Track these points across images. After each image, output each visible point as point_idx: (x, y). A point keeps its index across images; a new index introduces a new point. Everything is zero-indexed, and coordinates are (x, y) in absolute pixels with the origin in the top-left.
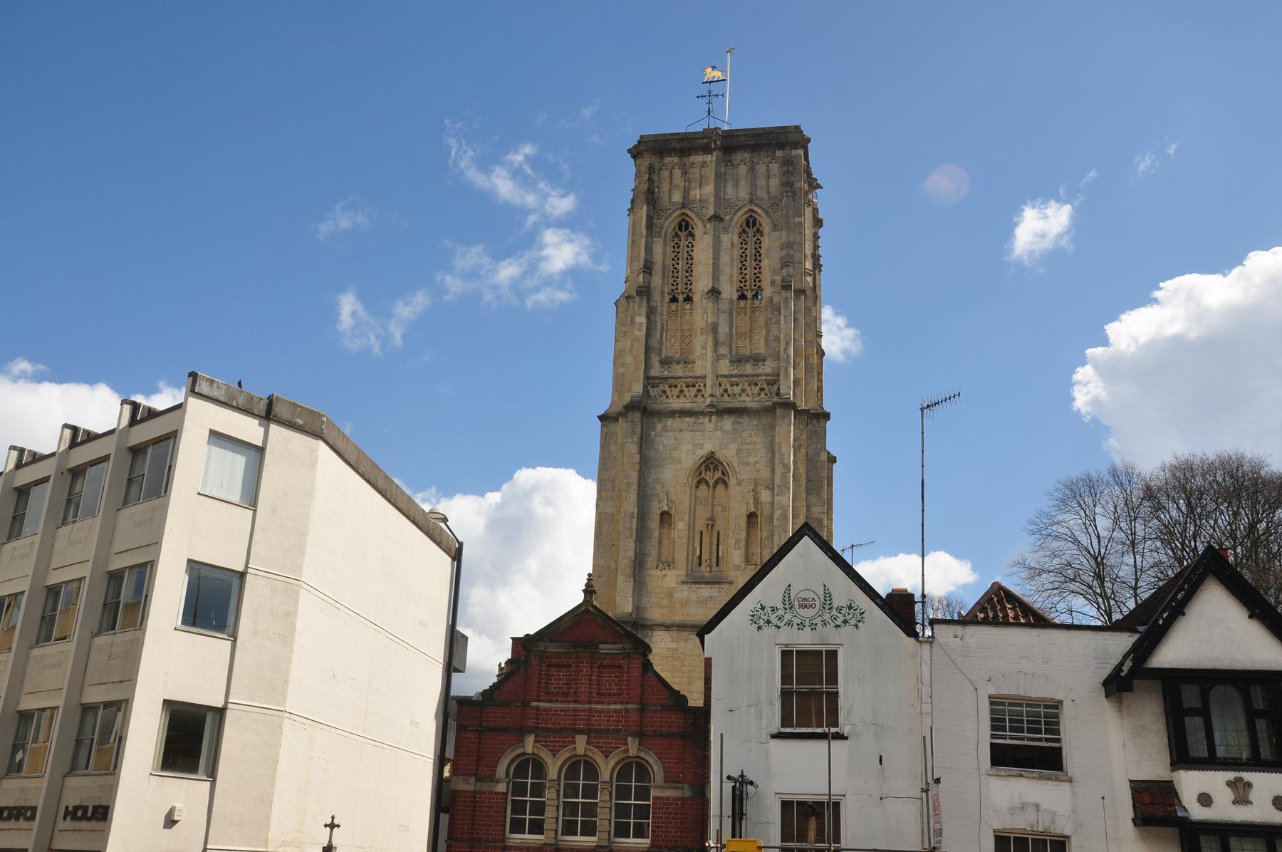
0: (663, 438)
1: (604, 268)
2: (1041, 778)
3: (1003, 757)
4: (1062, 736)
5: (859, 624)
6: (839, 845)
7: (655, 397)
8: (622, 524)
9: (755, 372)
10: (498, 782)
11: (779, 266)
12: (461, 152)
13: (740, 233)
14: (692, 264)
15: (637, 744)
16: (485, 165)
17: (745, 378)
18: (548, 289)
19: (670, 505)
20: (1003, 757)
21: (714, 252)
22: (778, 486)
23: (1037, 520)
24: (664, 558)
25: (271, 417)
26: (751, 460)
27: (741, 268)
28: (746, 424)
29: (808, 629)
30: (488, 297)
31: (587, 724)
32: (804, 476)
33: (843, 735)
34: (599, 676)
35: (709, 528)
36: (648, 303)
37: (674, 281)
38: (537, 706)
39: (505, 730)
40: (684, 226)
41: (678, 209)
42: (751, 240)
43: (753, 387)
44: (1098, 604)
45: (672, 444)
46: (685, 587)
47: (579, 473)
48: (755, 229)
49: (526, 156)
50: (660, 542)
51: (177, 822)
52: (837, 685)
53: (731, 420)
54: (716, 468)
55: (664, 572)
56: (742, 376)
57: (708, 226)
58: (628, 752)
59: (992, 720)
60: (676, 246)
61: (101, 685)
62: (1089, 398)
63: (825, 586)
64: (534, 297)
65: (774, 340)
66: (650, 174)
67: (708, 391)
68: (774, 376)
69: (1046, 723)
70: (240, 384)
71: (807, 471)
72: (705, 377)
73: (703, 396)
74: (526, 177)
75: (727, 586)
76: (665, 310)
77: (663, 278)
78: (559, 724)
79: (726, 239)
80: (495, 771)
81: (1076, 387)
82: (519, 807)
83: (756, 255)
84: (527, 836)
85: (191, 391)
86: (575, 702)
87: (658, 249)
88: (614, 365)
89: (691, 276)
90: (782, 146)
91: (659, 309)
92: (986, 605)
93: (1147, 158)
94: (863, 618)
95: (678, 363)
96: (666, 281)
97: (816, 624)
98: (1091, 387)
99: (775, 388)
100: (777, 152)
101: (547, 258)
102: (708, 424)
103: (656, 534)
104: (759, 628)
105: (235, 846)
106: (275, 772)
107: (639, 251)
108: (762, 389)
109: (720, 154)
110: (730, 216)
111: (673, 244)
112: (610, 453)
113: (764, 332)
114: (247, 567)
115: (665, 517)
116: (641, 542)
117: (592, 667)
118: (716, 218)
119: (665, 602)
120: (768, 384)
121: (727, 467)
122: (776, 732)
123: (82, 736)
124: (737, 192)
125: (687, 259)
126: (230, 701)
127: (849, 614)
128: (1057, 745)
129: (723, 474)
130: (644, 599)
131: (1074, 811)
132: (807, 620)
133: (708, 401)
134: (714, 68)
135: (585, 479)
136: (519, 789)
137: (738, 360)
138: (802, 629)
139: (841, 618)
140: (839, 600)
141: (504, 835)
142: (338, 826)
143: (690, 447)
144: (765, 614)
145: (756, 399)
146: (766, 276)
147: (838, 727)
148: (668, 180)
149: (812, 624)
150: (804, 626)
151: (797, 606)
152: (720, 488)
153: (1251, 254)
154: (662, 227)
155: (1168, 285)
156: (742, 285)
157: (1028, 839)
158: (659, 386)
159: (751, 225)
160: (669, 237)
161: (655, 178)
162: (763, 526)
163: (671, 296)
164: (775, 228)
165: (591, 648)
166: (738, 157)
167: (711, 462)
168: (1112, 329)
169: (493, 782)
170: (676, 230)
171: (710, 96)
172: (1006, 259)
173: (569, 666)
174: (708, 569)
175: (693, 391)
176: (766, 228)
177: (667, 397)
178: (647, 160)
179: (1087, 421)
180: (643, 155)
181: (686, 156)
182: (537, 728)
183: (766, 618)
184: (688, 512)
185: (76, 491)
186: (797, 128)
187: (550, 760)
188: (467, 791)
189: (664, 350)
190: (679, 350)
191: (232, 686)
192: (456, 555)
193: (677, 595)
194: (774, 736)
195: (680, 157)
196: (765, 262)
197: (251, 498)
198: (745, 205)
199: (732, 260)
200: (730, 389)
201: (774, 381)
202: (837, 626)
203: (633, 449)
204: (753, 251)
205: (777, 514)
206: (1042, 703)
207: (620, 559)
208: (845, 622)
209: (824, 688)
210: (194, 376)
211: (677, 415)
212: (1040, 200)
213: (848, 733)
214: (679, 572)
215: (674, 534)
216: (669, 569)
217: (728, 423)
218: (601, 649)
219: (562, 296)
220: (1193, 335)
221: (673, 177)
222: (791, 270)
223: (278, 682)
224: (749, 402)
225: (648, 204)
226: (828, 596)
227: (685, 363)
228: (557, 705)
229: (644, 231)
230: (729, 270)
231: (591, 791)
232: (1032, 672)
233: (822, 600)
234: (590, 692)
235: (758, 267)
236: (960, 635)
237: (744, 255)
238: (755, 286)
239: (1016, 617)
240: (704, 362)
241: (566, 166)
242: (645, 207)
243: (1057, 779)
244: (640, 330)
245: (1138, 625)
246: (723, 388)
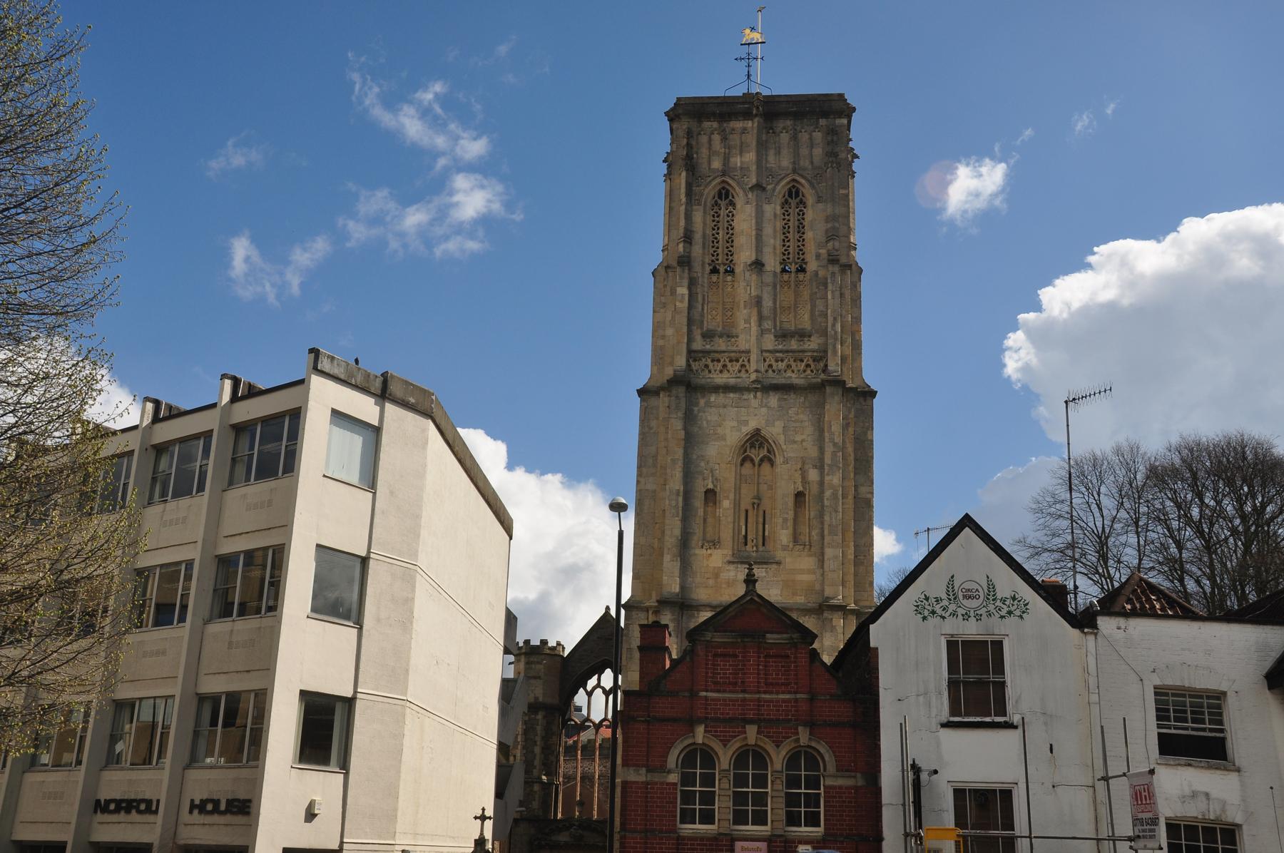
0: (706, 414)
1: (518, 217)
2: (1210, 767)
3: (1171, 747)
4: (1226, 726)
5: (1024, 615)
6: (1013, 832)
7: (697, 371)
8: (667, 502)
9: (801, 348)
10: (669, 772)
11: (824, 240)
12: (366, 88)
14: (733, 234)
15: (808, 733)
16: (392, 102)
17: (791, 354)
18: (459, 238)
19: (715, 483)
20: (1171, 747)
21: (757, 223)
22: (829, 465)
23: (1041, 499)
24: (709, 536)
25: (387, 395)
26: (798, 438)
27: (784, 240)
28: (792, 401)
29: (973, 620)
30: (394, 244)
31: (758, 714)
32: (852, 455)
33: (1012, 724)
34: (765, 666)
35: (755, 507)
36: (689, 274)
37: (714, 252)
38: (706, 697)
39: (674, 720)
40: (724, 194)
41: (718, 176)
42: (793, 211)
43: (799, 363)
44: (1102, 585)
45: (716, 421)
46: (732, 567)
47: (488, 434)
48: (798, 199)
49: (436, 94)
50: (705, 520)
51: (316, 815)
52: (1004, 675)
53: (777, 397)
54: (761, 446)
55: (709, 551)
56: (787, 351)
57: (750, 195)
58: (799, 742)
59: (1158, 710)
60: (716, 215)
61: (222, 675)
62: (1020, 364)
63: (988, 577)
64: (443, 247)
65: (820, 315)
66: (688, 139)
67: (753, 367)
68: (820, 352)
69: (1192, 712)
70: (357, 361)
71: (855, 450)
72: (748, 352)
73: (747, 371)
74: (436, 118)
75: (774, 566)
76: (706, 281)
77: (704, 247)
78: (728, 714)
79: (768, 209)
80: (666, 761)
81: (1007, 354)
82: (688, 797)
83: (799, 227)
84: (698, 826)
85: (313, 368)
86: (744, 691)
87: (698, 217)
88: (653, 337)
89: (732, 246)
90: (825, 114)
91: (700, 280)
92: (1131, 596)
93: (1085, 117)
94: (1027, 609)
95: (721, 336)
96: (706, 251)
97: (981, 615)
98: (1022, 353)
99: (822, 365)
100: (820, 120)
101: (457, 204)
102: (753, 400)
103: (701, 512)
104: (924, 618)
105: (367, 839)
106: (401, 763)
107: (679, 219)
108: (808, 366)
109: (761, 120)
110: (773, 185)
111: (712, 213)
112: (650, 428)
113: (809, 307)
114: (369, 552)
115: (711, 495)
116: (685, 521)
117: (759, 657)
118: (759, 187)
119: (711, 582)
120: (814, 361)
121: (773, 444)
122: (946, 721)
123: (199, 727)
124: (779, 160)
125: (728, 228)
126: (359, 690)
127: (1013, 605)
128: (1221, 735)
129: (769, 451)
130: (690, 579)
131: (1244, 801)
132: (972, 611)
133: (753, 377)
134: (752, 29)
135: (495, 440)
136: (687, 779)
137: (783, 335)
138: (967, 620)
139: (1005, 609)
140: (1003, 591)
141: (676, 825)
142: (476, 818)
143: (735, 424)
144: (929, 605)
145: (802, 376)
146: (811, 249)
147: (1006, 716)
148: (706, 145)
149: (977, 614)
150: (969, 617)
151: (961, 597)
152: (766, 466)
153: (1185, 220)
154: (702, 195)
155: (1102, 249)
156: (785, 257)
157: (1180, 825)
158: (700, 360)
159: (794, 196)
160: (709, 204)
161: (694, 143)
162: (811, 505)
163: (711, 267)
164: (819, 200)
165: (759, 638)
166: (779, 124)
167: (756, 439)
168: (1046, 294)
169: (664, 772)
170: (716, 198)
171: (749, 59)
172: (938, 218)
173: (735, 656)
174: (755, 549)
175: (737, 366)
176: (810, 200)
177: (710, 372)
178: (684, 125)
179: (1017, 388)
180: (680, 118)
181: (725, 121)
182: (707, 718)
183: (930, 608)
184: (733, 490)
185: (160, 471)
186: (841, 96)
187: (721, 750)
189: (705, 322)
190: (721, 323)
191: (360, 676)
194: (944, 725)
195: (719, 122)
196: (809, 235)
197: (370, 481)
198: (788, 175)
199: (775, 231)
200: (774, 364)
201: (821, 357)
202: (1002, 617)
203: (677, 425)
204: (797, 223)
205: (828, 493)
206: (1187, 693)
207: (667, 538)
208: (1010, 613)
209: (992, 677)
210: (315, 352)
211: (721, 391)
212: (974, 157)
213: (1017, 722)
214: (725, 552)
215: (720, 512)
216: (715, 548)
217: (773, 400)
218: (768, 639)
219: (473, 246)
220: (1126, 302)
221: (712, 142)
222: (837, 244)
223: (399, 673)
224: (795, 378)
225: (687, 170)
226: (991, 587)
227: (728, 336)
228: (726, 695)
229: (684, 200)
230: (772, 241)
231: (761, 781)
232: (1195, 664)
233: (986, 591)
234: (758, 682)
235: (801, 240)
236: (1123, 627)
237: (787, 226)
238: (798, 259)
239: (1163, 609)
240: (749, 335)
241: (479, 107)
242: (684, 174)
243: (1226, 769)
244: (682, 301)
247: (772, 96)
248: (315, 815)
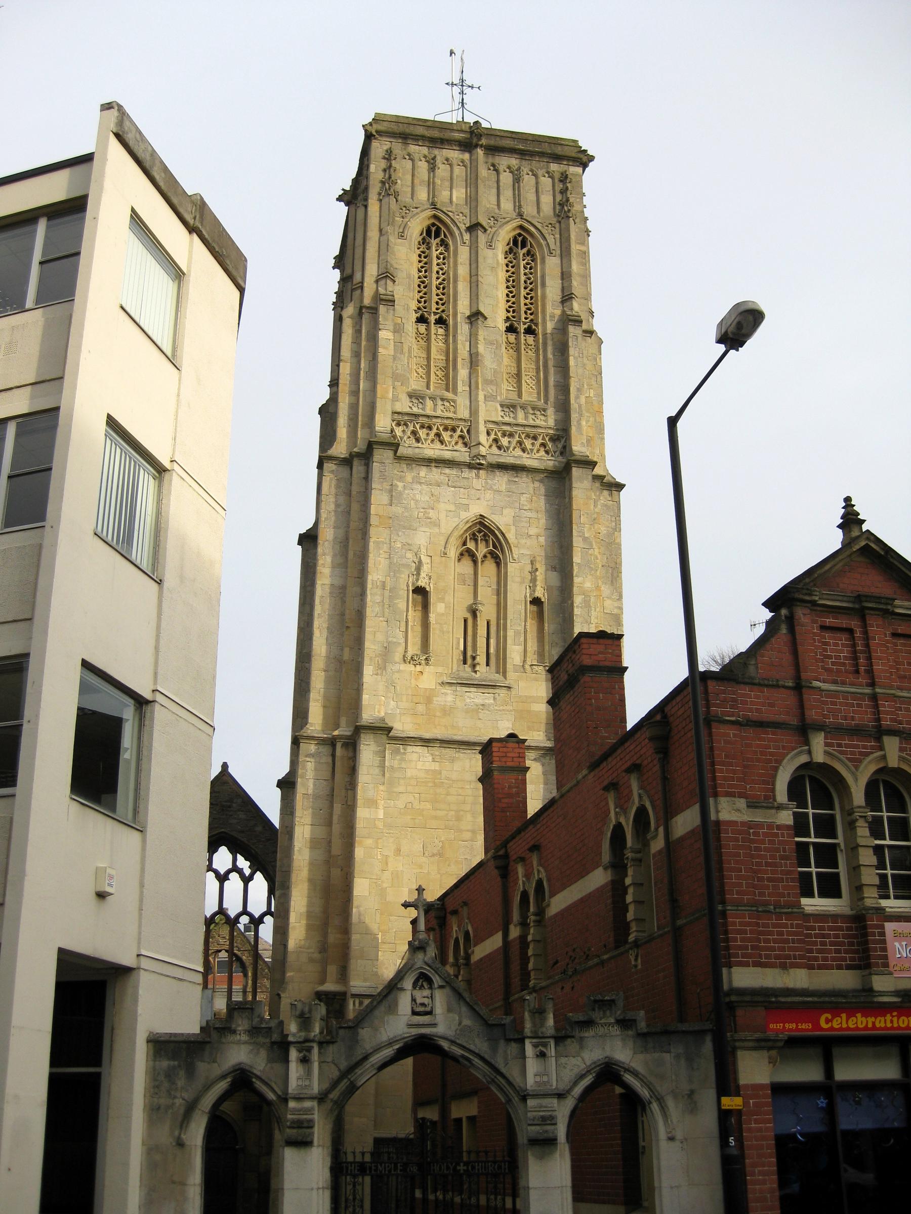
13: (506, 252)
27: (507, 295)
46: (448, 690)
48: (525, 250)
55: (419, 668)
78: (853, 718)
90: (557, 158)
129: (495, 546)
143: (452, 508)
170: (425, 235)
188: (736, 822)
192: (673, 422)
193: (438, 701)
246: (493, 436)
247: (491, 129)
248: (281, 784)
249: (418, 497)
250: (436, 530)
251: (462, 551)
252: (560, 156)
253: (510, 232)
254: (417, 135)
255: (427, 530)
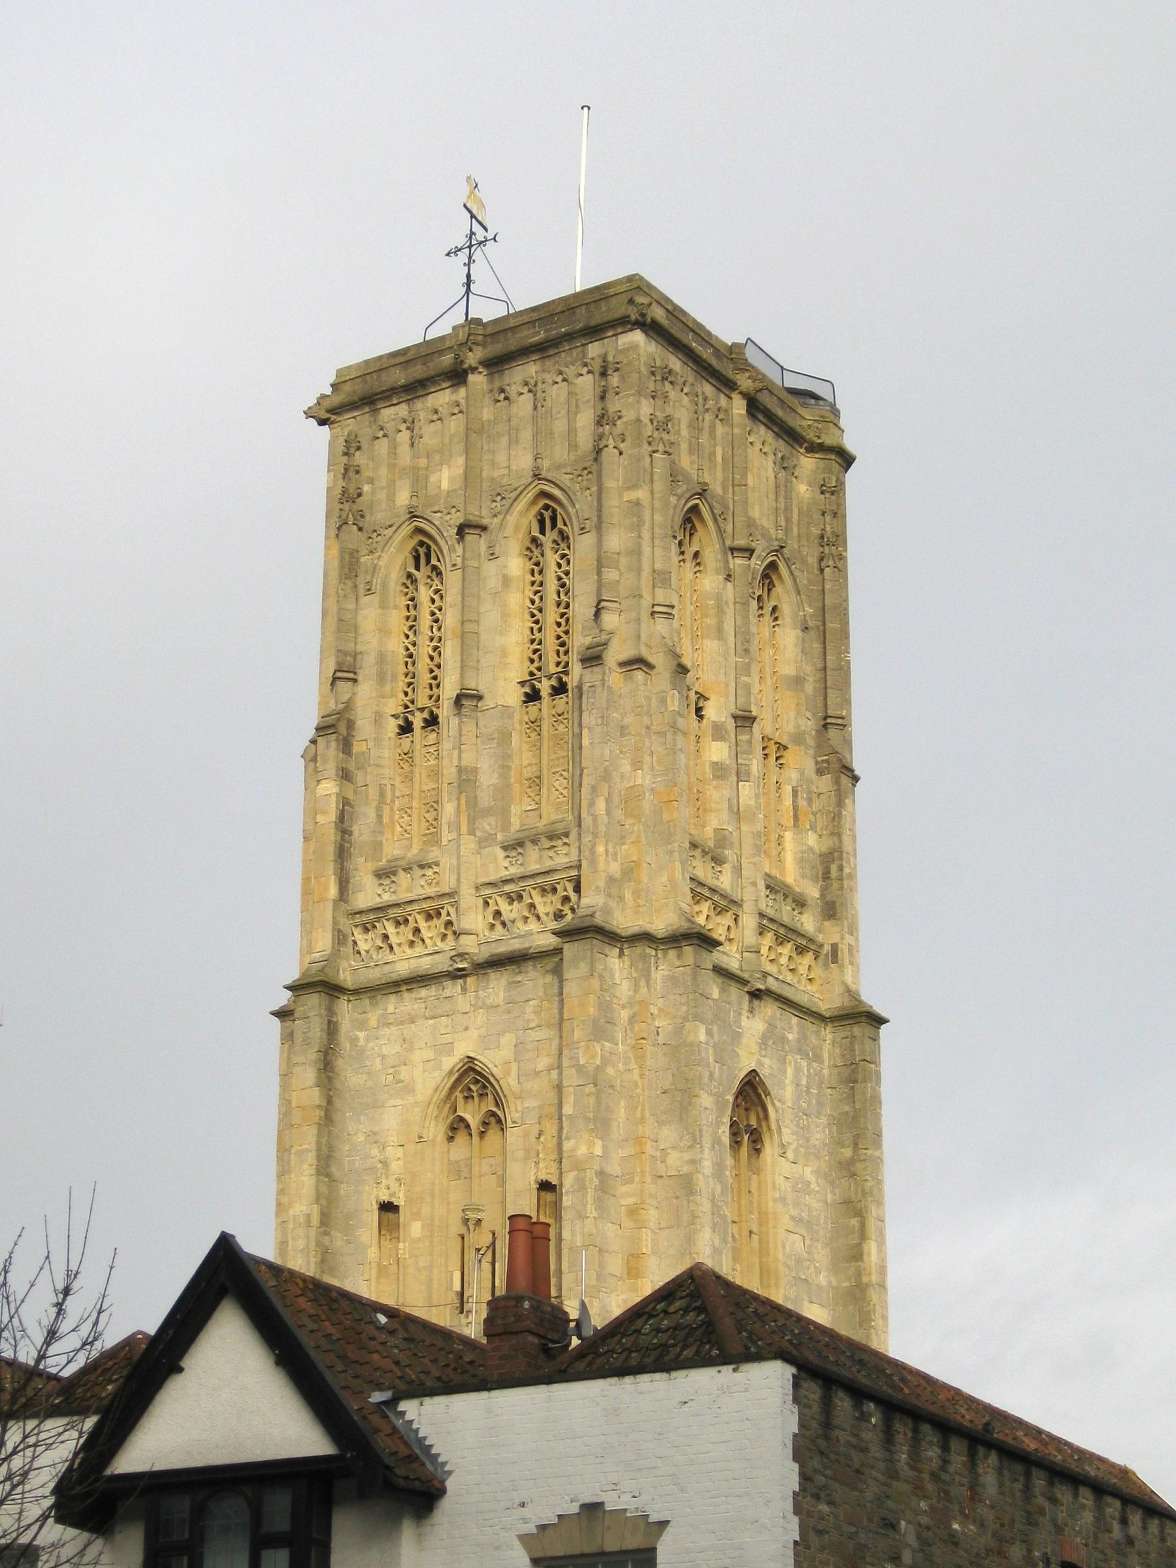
53: (503, 982)
137: (514, 846)
143: (429, 1054)
152: (493, 1134)
245: (421, 1391)
246: (492, 908)
249: (385, 1050)
250: (411, 1099)
251: (453, 1123)
252: (596, 326)
253: (528, 510)
254: (383, 392)
255: (398, 1102)
